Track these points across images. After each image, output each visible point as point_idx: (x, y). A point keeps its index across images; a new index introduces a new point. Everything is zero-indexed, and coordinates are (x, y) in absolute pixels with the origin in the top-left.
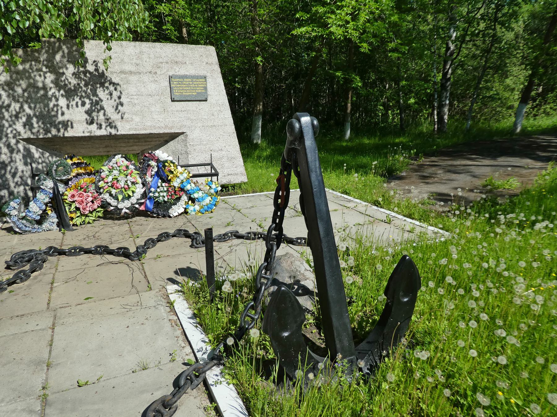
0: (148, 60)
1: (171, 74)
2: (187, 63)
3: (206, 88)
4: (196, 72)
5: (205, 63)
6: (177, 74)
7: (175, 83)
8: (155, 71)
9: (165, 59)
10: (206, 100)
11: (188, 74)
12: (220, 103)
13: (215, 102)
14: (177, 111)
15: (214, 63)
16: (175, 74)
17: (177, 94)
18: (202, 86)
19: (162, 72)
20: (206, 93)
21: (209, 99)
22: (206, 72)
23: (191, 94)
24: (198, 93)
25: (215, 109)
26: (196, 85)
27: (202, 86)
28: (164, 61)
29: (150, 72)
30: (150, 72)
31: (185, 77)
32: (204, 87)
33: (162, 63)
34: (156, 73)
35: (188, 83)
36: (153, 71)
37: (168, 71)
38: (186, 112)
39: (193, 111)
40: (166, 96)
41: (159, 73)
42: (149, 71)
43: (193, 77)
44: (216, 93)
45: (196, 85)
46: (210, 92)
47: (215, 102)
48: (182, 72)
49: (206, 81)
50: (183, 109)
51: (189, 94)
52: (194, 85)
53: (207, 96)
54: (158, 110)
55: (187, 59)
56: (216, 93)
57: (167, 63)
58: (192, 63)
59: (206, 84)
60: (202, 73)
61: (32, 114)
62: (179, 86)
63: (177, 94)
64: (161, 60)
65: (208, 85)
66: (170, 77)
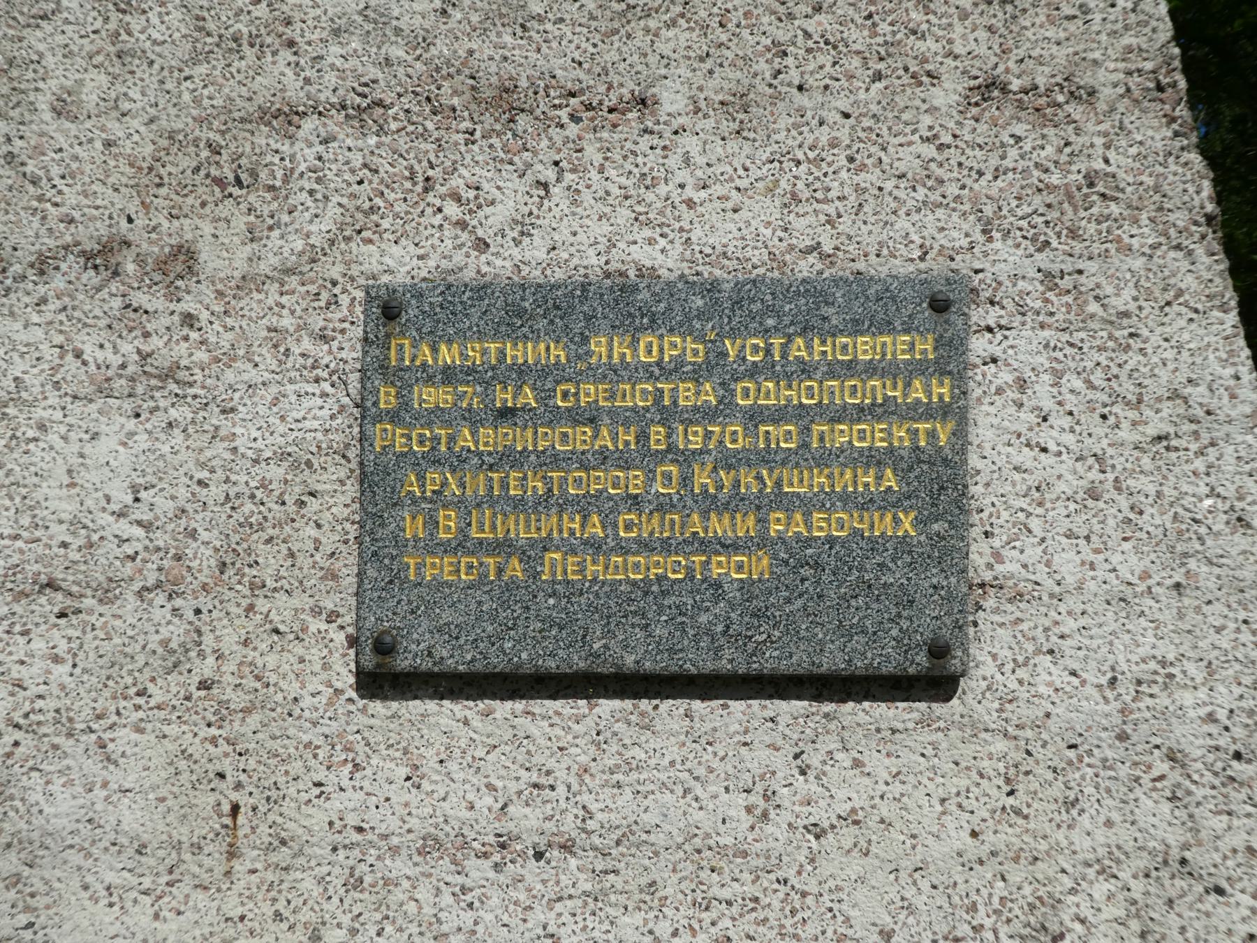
0: (94, 87)
1: (397, 262)
2: (672, 100)
3: (939, 484)
4: (805, 227)
5: (947, 95)
6: (499, 264)
7: (431, 396)
8: (172, 232)
9: (343, 64)
10: (935, 681)
11: (666, 259)
12: (1191, 738)
13: (1092, 709)
14: (430, 846)
15: (1106, 79)
16: (472, 266)
17: (439, 568)
18: (877, 435)
19: (283, 247)
20: (947, 551)
21: (989, 653)
22: (961, 231)
23: (672, 568)
24: (799, 559)
25: (1088, 836)
26: (784, 436)
27: (877, 435)
28: (328, 87)
29: (103, 257)
30: (103, 257)
31: (625, 301)
32: (910, 462)
33: (285, 117)
34: (180, 263)
35: (637, 396)
36: (154, 231)
37: (360, 225)
38: (573, 873)
39: (701, 851)
40: (282, 609)
41: (222, 255)
42: (90, 234)
43: (730, 305)
44: (1128, 562)
45: (784, 436)
46: (999, 547)
47: (1092, 709)
48: (569, 221)
49: (950, 361)
50: (527, 820)
51: (642, 567)
52: (735, 436)
53: (963, 600)
54: (131, 817)
55: (677, 39)
56: (1128, 562)
57: (364, 110)
58: (738, 103)
59: (955, 412)
60: (898, 238)
61: (996, 566)
62: (489, 438)
63: (439, 568)
64: (279, 77)
65: (991, 424)
66: (382, 678)
